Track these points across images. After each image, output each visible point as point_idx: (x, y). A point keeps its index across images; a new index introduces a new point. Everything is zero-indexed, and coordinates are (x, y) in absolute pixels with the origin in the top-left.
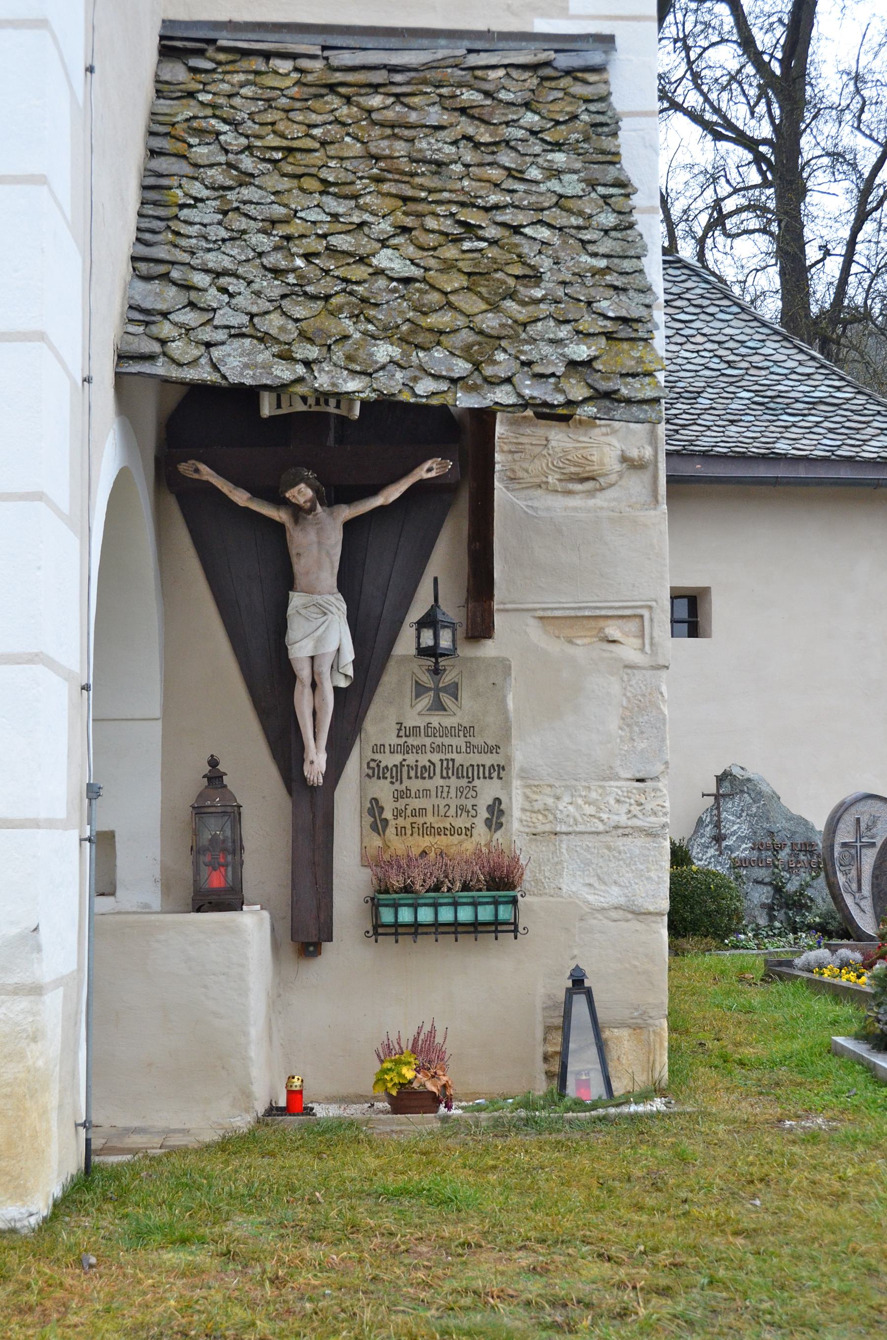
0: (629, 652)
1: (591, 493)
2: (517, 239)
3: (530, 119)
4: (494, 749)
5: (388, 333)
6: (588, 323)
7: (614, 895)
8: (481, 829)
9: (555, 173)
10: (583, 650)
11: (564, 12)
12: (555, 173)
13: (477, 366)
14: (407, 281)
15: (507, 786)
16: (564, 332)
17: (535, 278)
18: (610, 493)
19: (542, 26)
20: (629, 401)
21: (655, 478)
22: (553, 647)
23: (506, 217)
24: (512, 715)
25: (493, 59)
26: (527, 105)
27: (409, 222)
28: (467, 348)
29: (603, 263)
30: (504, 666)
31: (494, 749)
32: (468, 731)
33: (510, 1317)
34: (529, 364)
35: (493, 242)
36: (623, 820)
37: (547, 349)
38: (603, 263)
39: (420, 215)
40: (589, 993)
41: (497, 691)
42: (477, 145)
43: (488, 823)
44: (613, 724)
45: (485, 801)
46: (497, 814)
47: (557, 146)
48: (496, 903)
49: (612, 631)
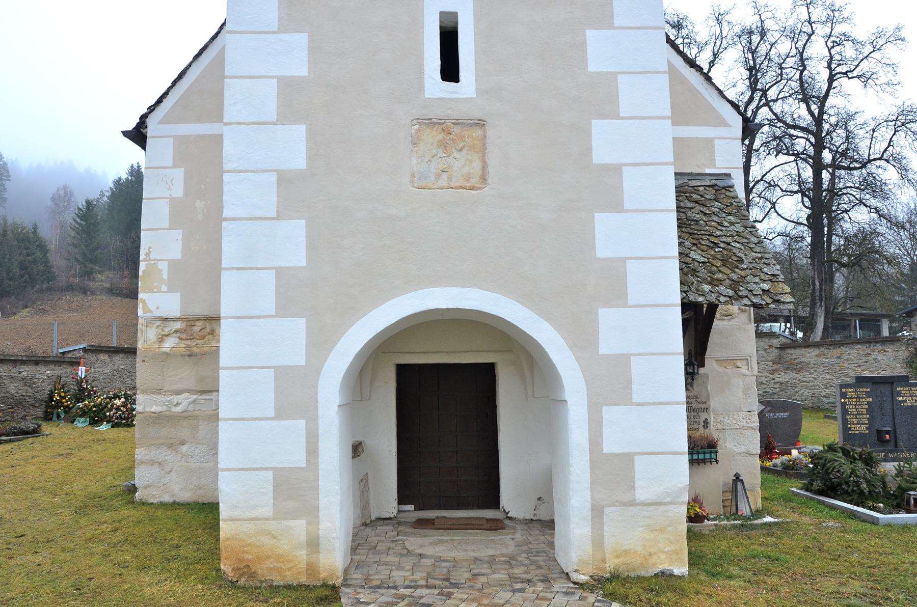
0: (744, 370)
1: (729, 320)
2: (730, 247)
3: (717, 204)
4: (704, 403)
5: (704, 281)
6: (763, 276)
7: (743, 449)
8: (701, 428)
9: (732, 224)
10: (730, 370)
11: (714, 166)
12: (732, 224)
13: (735, 292)
14: (703, 263)
15: (709, 414)
16: (757, 280)
17: (742, 261)
18: (736, 320)
19: (708, 171)
20: (784, 303)
21: (750, 315)
22: (721, 370)
23: (724, 239)
24: (141, 273)
25: (699, 184)
26: (715, 200)
27: (695, 241)
28: (730, 286)
29: (759, 255)
30: (707, 376)
31: (704, 403)
32: (696, 397)
33: (854, 601)
34: (751, 291)
35: (723, 248)
36: (745, 424)
37: (755, 286)
38: (759, 255)
39: (697, 239)
40: (742, 481)
41: (705, 383)
42: (705, 214)
43: (704, 426)
44: (740, 394)
45: (702, 419)
46: (706, 424)
47: (730, 214)
48: (711, 452)
49: (739, 364)
